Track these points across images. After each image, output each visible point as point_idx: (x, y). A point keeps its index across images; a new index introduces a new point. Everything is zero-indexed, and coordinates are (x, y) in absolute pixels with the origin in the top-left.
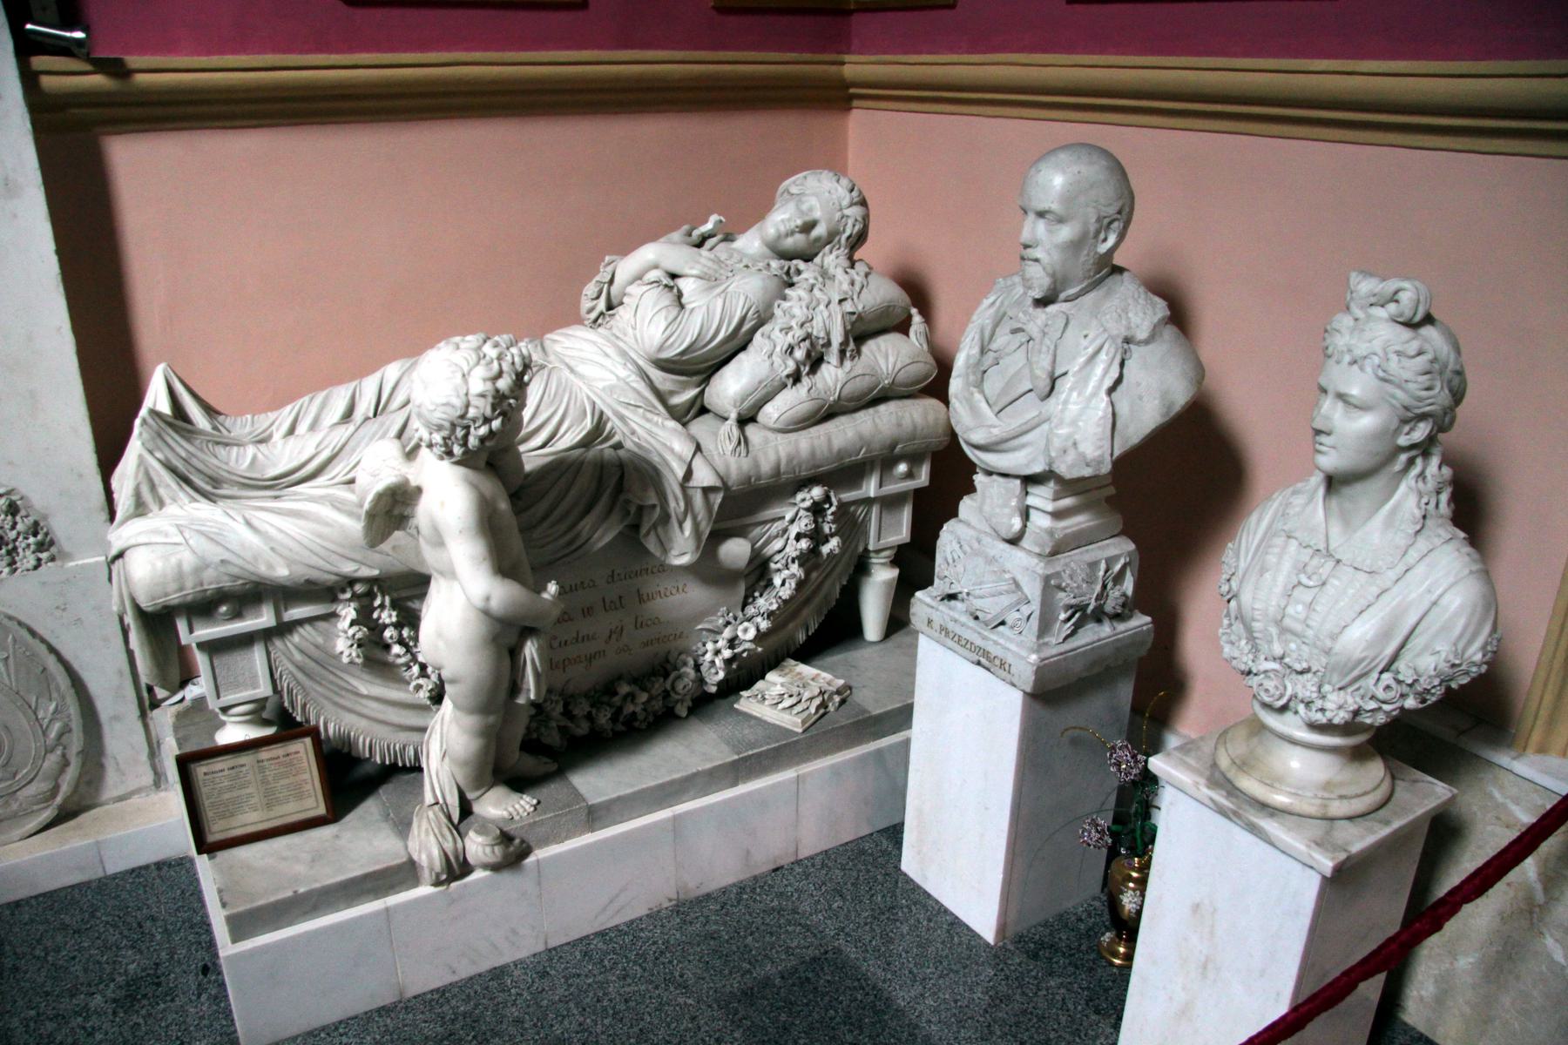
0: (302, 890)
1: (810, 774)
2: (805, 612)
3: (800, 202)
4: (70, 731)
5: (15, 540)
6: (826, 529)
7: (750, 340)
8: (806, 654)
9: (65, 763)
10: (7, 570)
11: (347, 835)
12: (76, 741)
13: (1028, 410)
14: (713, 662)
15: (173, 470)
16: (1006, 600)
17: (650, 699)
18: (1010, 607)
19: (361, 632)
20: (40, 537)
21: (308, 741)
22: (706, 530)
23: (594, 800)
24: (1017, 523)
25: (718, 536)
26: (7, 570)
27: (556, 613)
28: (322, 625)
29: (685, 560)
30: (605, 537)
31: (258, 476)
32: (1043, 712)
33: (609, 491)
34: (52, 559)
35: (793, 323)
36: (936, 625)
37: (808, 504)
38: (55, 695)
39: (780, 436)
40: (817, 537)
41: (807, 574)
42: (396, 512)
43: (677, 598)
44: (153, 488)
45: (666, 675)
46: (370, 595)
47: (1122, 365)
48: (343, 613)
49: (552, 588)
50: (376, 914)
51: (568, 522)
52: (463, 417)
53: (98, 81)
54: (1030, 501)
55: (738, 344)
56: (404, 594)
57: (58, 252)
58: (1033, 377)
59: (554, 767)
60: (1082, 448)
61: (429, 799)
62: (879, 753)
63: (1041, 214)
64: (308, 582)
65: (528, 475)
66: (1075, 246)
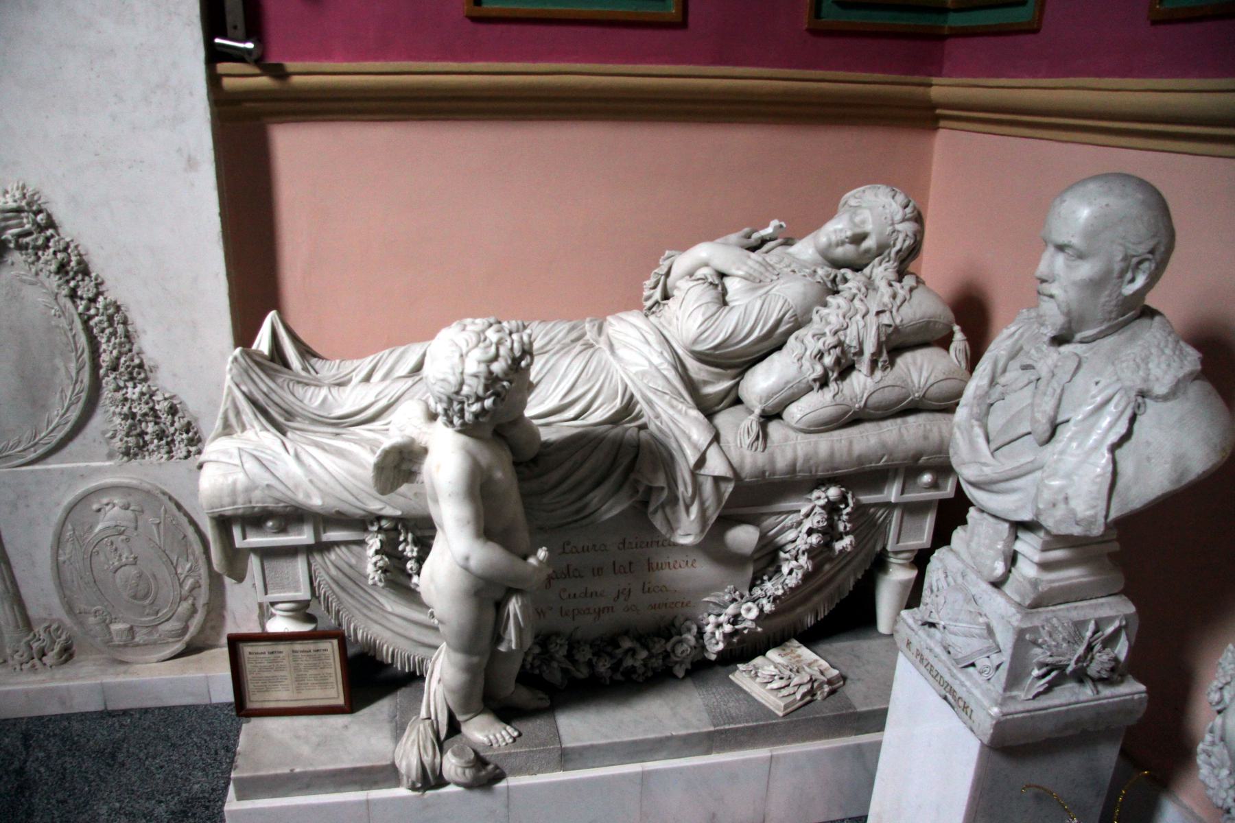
0: (298, 770)
1: (785, 756)
3: (855, 214)
5: (173, 434)
6: (841, 527)
7: (784, 343)
8: (810, 638)
9: (194, 611)
10: (166, 456)
11: (354, 728)
12: (203, 596)
13: (1025, 453)
14: (713, 634)
16: (977, 644)
17: (651, 656)
18: (981, 652)
19: (384, 561)
21: (335, 642)
22: (713, 516)
23: (568, 743)
24: (999, 568)
25: (727, 520)
26: (166, 456)
27: (543, 576)
28: (355, 548)
30: (613, 509)
32: (1003, 764)
35: (827, 330)
36: (914, 649)
37: (822, 502)
38: (191, 557)
39: (801, 435)
40: (830, 533)
43: (684, 571)
44: (238, 413)
45: (668, 639)
47: (1133, 419)
48: (371, 542)
49: (542, 553)
50: (359, 803)
51: (582, 490)
52: (458, 393)
53: (264, 81)
54: (1019, 546)
55: (772, 343)
57: (221, 214)
58: (1034, 421)
59: (547, 703)
60: (1073, 503)
61: (423, 714)
63: (1061, 248)
64: (338, 512)
65: (547, 445)
66: (1095, 285)
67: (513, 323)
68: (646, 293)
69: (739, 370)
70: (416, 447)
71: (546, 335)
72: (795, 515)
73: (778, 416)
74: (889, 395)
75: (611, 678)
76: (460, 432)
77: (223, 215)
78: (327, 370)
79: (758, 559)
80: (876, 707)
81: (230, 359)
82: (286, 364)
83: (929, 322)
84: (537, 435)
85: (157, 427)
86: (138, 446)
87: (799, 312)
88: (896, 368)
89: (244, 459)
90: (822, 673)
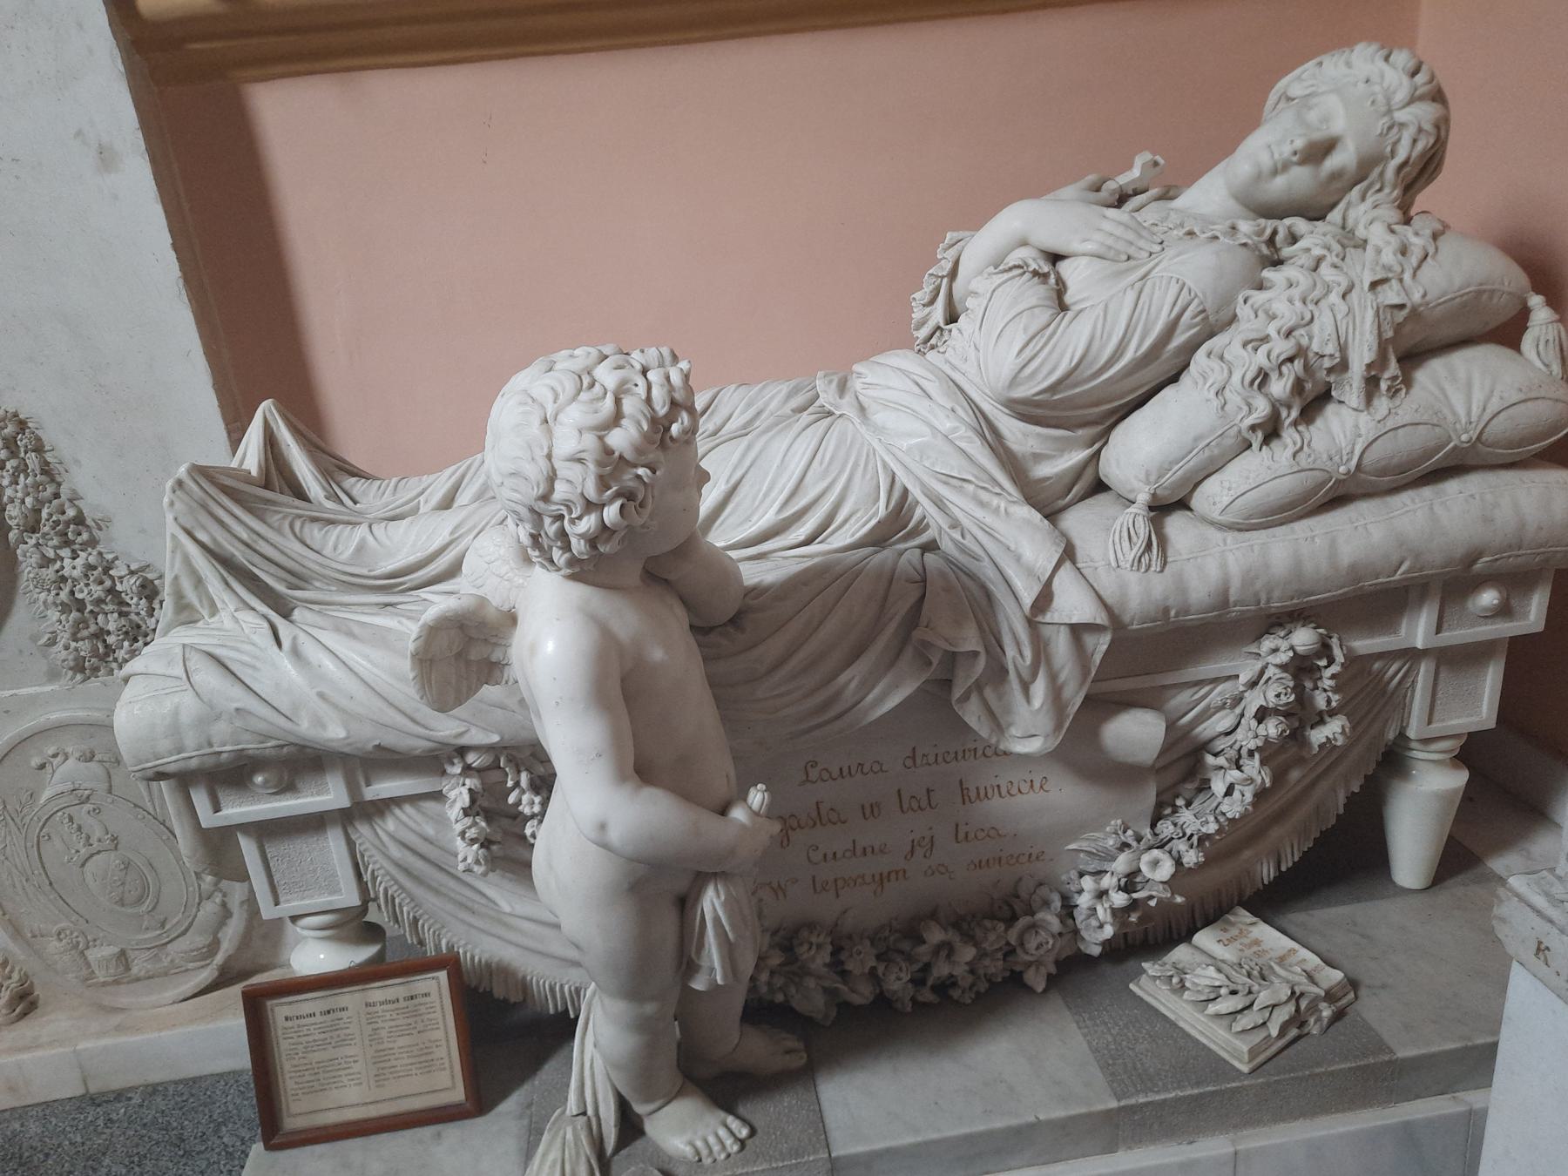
2: (1276, 833)
6: (1320, 701)
7: (1186, 366)
8: (1270, 902)
9: (226, 913)
17: (983, 954)
22: (1075, 697)
25: (1103, 703)
28: (429, 806)
29: (1033, 746)
31: (365, 572)
33: (893, 626)
35: (1271, 330)
37: (1284, 657)
39: (1231, 536)
40: (1300, 715)
41: (1279, 777)
42: (474, 655)
43: (1028, 801)
44: (199, 582)
45: (1012, 919)
48: (452, 795)
49: (757, 797)
52: (545, 498)
55: (1162, 370)
57: (175, 246)
59: (799, 1060)
65: (756, 591)
67: (652, 352)
68: (917, 315)
69: (1099, 428)
70: (491, 614)
71: (749, 406)
72: (1227, 685)
73: (1183, 504)
74: (1405, 444)
75: (913, 999)
76: (573, 577)
78: (372, 497)
79: (1165, 768)
80: (1435, 1049)
81: (169, 484)
82: (300, 493)
83: (1479, 293)
84: (737, 576)
85: (123, 621)
86: (94, 652)
87: (1209, 306)
88: (1415, 390)
89: (191, 665)
90: (1311, 978)
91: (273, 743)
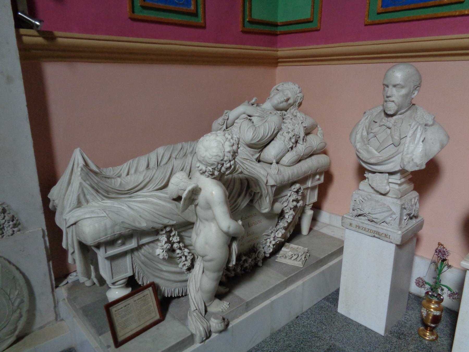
4: (24, 302)
5: (4, 224)
15: (93, 188)
18: (388, 216)
20: (14, 222)
28: (151, 245)
31: (123, 189)
34: (19, 230)
35: (290, 130)
36: (354, 225)
39: (288, 167)
44: (85, 195)
45: (255, 252)
46: (171, 231)
48: (162, 239)
52: (222, 160)
53: (40, 40)
54: (390, 180)
55: (272, 139)
56: (180, 230)
57: (28, 106)
60: (415, 161)
62: (323, 272)
63: (395, 86)
72: (286, 197)
74: (308, 151)
77: (28, 106)
91: (128, 230)
